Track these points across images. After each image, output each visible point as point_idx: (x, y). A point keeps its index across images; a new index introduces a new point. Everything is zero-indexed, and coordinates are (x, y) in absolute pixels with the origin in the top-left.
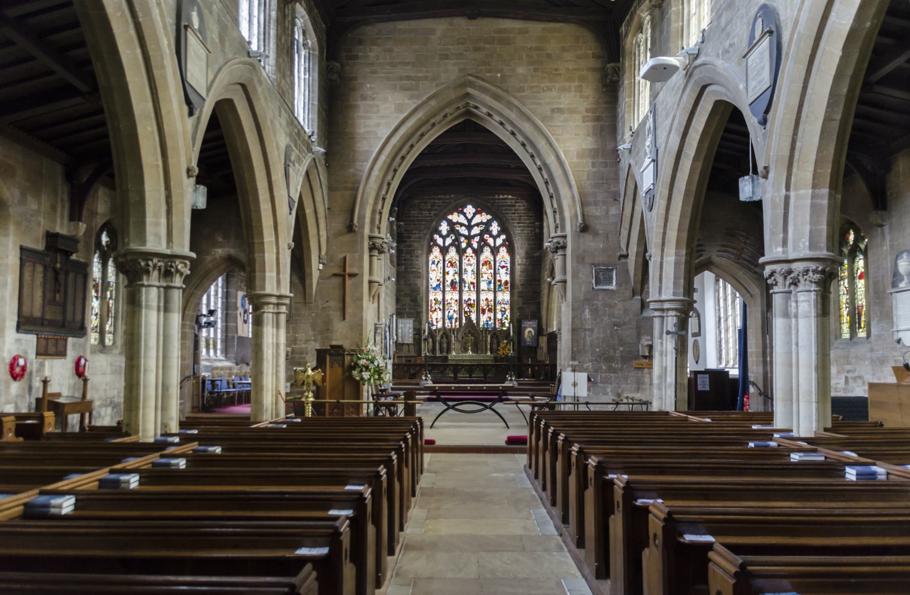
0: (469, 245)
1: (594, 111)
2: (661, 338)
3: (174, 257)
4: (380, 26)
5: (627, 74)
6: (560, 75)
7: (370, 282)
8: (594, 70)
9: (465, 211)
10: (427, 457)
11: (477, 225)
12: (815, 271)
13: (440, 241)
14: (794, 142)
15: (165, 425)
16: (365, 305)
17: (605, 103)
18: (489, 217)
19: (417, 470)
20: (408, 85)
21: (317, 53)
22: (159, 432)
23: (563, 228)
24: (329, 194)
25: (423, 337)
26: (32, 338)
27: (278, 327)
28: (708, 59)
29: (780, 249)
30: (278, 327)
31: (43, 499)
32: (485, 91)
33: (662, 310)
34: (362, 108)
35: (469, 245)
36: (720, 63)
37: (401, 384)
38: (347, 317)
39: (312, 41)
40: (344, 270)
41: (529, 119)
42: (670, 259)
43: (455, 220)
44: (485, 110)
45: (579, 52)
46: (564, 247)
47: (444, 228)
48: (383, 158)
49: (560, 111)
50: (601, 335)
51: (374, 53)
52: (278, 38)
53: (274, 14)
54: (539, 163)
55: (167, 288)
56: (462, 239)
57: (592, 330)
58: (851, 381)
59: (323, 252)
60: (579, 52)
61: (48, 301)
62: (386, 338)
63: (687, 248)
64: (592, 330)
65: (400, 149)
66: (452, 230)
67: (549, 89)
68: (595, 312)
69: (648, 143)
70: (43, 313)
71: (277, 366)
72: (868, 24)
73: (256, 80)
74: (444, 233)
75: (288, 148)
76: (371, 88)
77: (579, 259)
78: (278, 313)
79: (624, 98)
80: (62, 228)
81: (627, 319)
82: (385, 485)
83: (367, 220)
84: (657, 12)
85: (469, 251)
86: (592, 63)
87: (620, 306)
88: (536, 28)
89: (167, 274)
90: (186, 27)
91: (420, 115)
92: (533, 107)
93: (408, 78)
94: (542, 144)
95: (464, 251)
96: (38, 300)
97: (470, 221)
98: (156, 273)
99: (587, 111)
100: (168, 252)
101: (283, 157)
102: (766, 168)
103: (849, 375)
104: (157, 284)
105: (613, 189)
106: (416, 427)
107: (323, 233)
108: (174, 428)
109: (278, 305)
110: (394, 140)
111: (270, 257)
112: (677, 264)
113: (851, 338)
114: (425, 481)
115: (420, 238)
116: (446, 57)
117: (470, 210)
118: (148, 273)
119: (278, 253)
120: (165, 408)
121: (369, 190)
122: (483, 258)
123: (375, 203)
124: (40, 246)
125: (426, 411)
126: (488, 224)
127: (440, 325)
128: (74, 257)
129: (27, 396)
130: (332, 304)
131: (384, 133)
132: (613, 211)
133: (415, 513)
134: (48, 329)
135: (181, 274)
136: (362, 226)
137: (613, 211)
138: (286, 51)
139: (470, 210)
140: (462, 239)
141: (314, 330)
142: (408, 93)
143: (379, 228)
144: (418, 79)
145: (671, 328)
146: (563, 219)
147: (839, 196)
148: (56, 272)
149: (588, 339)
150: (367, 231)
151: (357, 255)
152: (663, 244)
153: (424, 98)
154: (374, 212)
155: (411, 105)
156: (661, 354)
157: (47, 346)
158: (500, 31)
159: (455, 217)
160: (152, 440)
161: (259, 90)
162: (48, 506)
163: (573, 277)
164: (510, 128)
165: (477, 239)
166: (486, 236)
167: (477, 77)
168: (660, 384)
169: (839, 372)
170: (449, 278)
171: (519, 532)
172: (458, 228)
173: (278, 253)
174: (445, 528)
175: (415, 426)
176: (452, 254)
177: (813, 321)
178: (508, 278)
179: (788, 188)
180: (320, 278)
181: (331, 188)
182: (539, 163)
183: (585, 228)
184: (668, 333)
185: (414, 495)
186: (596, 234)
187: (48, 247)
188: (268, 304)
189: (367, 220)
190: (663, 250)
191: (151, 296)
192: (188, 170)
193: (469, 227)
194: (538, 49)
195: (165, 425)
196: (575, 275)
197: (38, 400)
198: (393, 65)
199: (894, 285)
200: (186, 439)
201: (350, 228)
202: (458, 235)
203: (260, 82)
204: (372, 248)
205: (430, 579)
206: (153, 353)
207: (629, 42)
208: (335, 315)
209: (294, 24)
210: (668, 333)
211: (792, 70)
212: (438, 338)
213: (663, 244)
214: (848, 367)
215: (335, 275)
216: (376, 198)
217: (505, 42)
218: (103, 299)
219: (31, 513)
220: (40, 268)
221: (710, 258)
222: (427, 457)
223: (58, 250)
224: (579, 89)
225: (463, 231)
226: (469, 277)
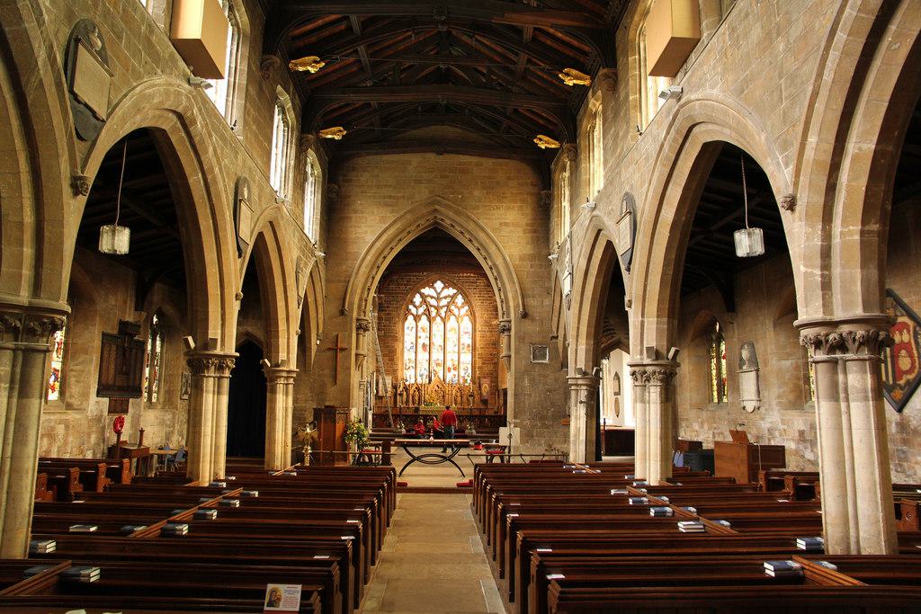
0: (438, 314)
1: (532, 225)
2: (576, 406)
3: (226, 356)
4: (370, 158)
5: (556, 200)
6: (506, 197)
7: (357, 355)
8: (532, 194)
9: (435, 285)
10: (399, 496)
11: (445, 298)
12: (659, 373)
13: (413, 310)
14: (645, 286)
15: (216, 474)
16: (352, 374)
17: (541, 219)
18: (455, 291)
19: (391, 507)
20: (389, 202)
21: (321, 180)
22: (212, 479)
23: (508, 315)
24: (326, 285)
25: (399, 392)
26: (106, 400)
27: (287, 395)
28: (599, 214)
29: (639, 357)
30: (287, 395)
31: (170, 526)
32: (446, 206)
33: (577, 385)
34: (353, 219)
35: (438, 314)
36: (605, 219)
37: (379, 431)
38: (338, 382)
39: (318, 171)
40: (337, 345)
41: (483, 229)
42: (582, 347)
43: (426, 294)
44: (448, 222)
45: (520, 181)
46: (509, 330)
47: (417, 299)
48: (369, 257)
49: (506, 224)
50: (537, 399)
51: (364, 178)
52: (295, 178)
53: (292, 163)
54: (490, 264)
55: (220, 378)
56: (432, 309)
57: (530, 395)
58: (717, 436)
59: (321, 331)
60: (520, 181)
61: (118, 372)
62: (367, 393)
63: (594, 340)
64: (530, 395)
65: (382, 251)
66: (424, 301)
67: (498, 208)
68: (532, 381)
69: (567, 259)
70: (115, 382)
71: (286, 424)
72: (684, 218)
73: (279, 216)
74: (417, 304)
75: (299, 259)
76: (361, 204)
77: (521, 339)
78: (287, 384)
79: (554, 220)
80: (130, 317)
81: (557, 387)
82: (370, 520)
83: (356, 306)
84: (573, 163)
85: (438, 318)
86: (530, 189)
87: (552, 376)
88: (488, 162)
89: (220, 368)
90: (240, 201)
91: (399, 225)
92: (485, 221)
93: (390, 197)
94: (492, 249)
95: (434, 318)
96: (112, 371)
97: (439, 294)
98: (213, 367)
99: (527, 225)
100: (222, 353)
101: (295, 267)
102: (630, 301)
103: (716, 431)
104: (213, 375)
105: (546, 285)
106: (389, 474)
107: (321, 316)
108: (222, 476)
109: (287, 378)
110: (378, 245)
111: (282, 341)
112: (587, 351)
113: (719, 403)
114: (397, 516)
115: (397, 308)
116: (418, 181)
117: (439, 285)
118: (208, 368)
119: (288, 338)
120: (216, 462)
121: (358, 282)
122: (449, 325)
123: (362, 293)
124: (115, 332)
125: (398, 458)
126: (453, 297)
127: (413, 381)
128: (136, 338)
129: (102, 445)
130: (327, 372)
131: (370, 238)
132: (547, 302)
133: (389, 538)
134: (118, 393)
135: (229, 368)
136: (351, 310)
137: (547, 302)
138: (300, 187)
139: (439, 285)
140: (432, 309)
141: (311, 392)
142: (390, 209)
143: (364, 312)
144: (398, 198)
145: (584, 399)
146: (508, 307)
147: (676, 322)
148: (124, 350)
149: (527, 403)
150: (355, 315)
151: (347, 333)
152: (577, 336)
153: (402, 213)
154: (361, 299)
155: (391, 218)
156: (576, 418)
157: (115, 406)
158: (460, 164)
159: (426, 291)
160: (207, 485)
161: (281, 223)
162: (175, 530)
163: (515, 354)
164: (468, 236)
165: (445, 309)
166: (452, 307)
167: (443, 198)
168: (575, 441)
169: (709, 429)
170: (420, 342)
171: (459, 551)
172: (429, 299)
173: (288, 338)
174: (410, 548)
175: (390, 475)
176: (424, 321)
177: (659, 406)
178: (470, 342)
179: (643, 316)
180: (317, 351)
181: (328, 281)
182: (490, 264)
183: (525, 315)
184: (581, 402)
185: (388, 526)
186: (533, 320)
187: (120, 331)
188: (281, 377)
189: (356, 306)
190: (577, 341)
191: (209, 384)
192: (237, 296)
193: (438, 299)
194: (490, 178)
195: (216, 474)
196: (517, 353)
197: (110, 449)
198: (379, 187)
199: (741, 368)
200: (232, 485)
201: (342, 312)
202: (428, 306)
203: (282, 217)
204: (359, 328)
205: (398, 579)
206: (209, 423)
207: (556, 176)
208: (328, 381)
209: (306, 164)
210: (581, 402)
211: (642, 239)
212: (411, 392)
213: (577, 336)
214: (715, 425)
215: (329, 349)
216: (363, 289)
217: (464, 172)
218: (152, 366)
219: (165, 533)
220: (114, 348)
221: (620, 339)
222: (399, 496)
223: (127, 334)
224: (521, 208)
225: (433, 302)
226: (438, 340)
